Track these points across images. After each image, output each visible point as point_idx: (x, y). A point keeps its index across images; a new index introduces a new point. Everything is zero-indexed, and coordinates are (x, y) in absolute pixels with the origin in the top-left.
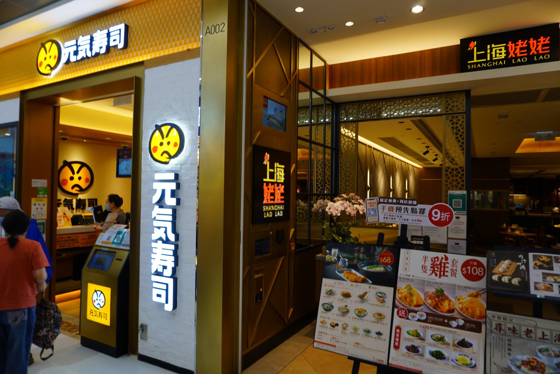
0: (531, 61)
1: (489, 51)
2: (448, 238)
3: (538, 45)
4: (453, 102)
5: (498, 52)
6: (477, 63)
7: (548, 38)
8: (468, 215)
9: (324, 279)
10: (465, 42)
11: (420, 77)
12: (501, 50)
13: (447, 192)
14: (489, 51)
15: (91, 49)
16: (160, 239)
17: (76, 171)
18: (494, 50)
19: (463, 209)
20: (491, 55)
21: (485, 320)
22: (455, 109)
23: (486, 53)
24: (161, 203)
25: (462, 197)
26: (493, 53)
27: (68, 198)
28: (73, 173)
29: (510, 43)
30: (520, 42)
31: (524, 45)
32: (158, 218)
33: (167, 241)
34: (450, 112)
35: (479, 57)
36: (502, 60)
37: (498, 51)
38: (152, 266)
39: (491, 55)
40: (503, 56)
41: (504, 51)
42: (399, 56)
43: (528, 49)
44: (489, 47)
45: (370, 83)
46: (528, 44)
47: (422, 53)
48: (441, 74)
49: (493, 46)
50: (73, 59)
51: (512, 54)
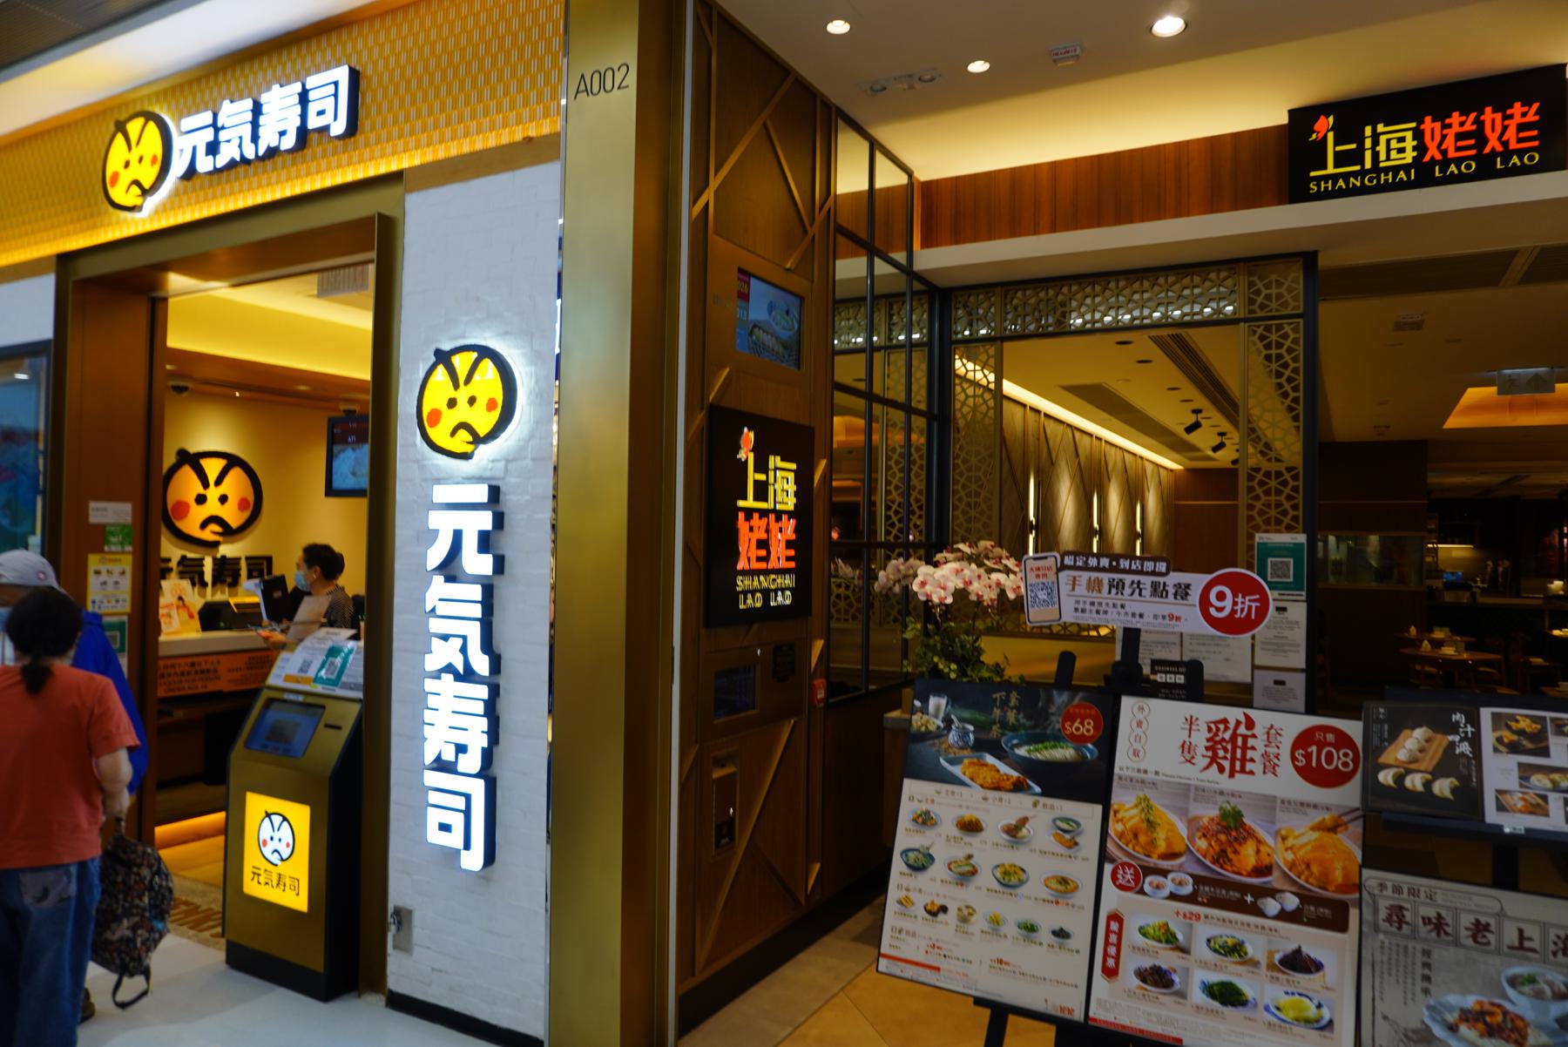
0: (1486, 170)
1: (1368, 143)
2: (1254, 667)
3: (1506, 126)
4: (1268, 286)
5: (1395, 144)
6: (1335, 177)
7: (1535, 106)
8: (1309, 601)
9: (907, 782)
10: (1302, 117)
11: (1177, 215)
12: (1402, 140)
13: (1251, 537)
14: (1368, 143)
15: (255, 138)
16: (449, 669)
18: (1383, 139)
19: (1296, 585)
20: (1375, 155)
21: (1357, 895)
22: (1274, 305)
23: (1361, 148)
24: (450, 568)
25: (1293, 550)
26: (1382, 148)
27: (190, 555)
28: (206, 485)
29: (1428, 119)
30: (1456, 118)
31: (1468, 127)
32: (442, 609)
33: (467, 675)
34: (1260, 314)
35: (1341, 159)
36: (1406, 168)
37: (1394, 144)
38: (426, 744)
39: (1375, 155)
40: (1409, 156)
41: (1410, 143)
42: (1117, 156)
43: (1479, 136)
44: (1368, 130)
45: (1036, 232)
46: (1479, 123)
47: (1180, 147)
48: (1235, 207)
49: (1380, 128)
50: (205, 164)
51: (1433, 152)
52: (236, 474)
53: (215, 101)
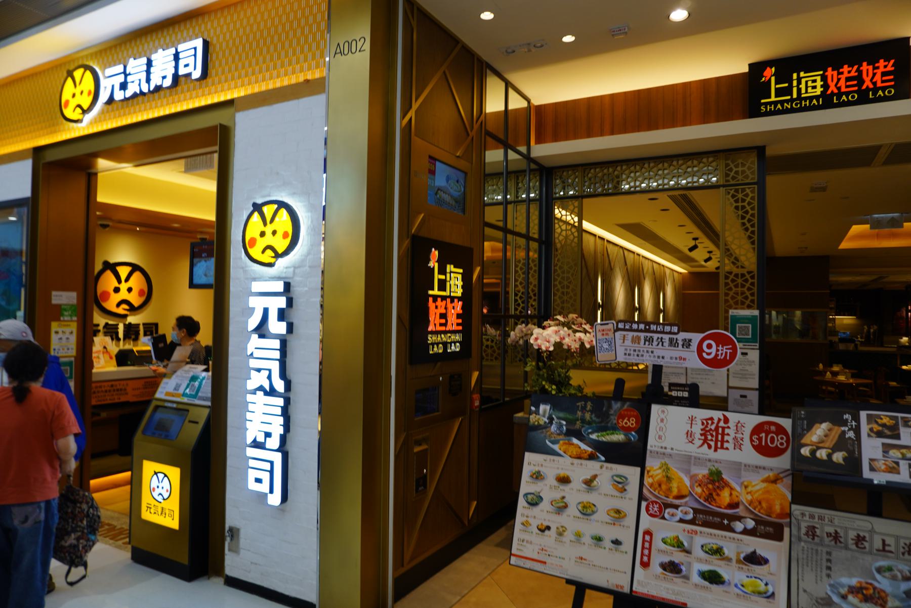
0: (864, 99)
1: (795, 83)
2: (729, 387)
3: (875, 73)
4: (737, 166)
5: (811, 84)
6: (776, 103)
7: (892, 62)
8: (761, 349)
9: (527, 454)
10: (757, 68)
11: (684, 125)
12: (814, 81)
13: (727, 312)
14: (795, 83)
15: (148, 80)
16: (261, 388)
17: (123, 277)
18: (803, 81)
19: (753, 340)
20: (799, 90)
21: (788, 520)
22: (740, 177)
23: (791, 86)
24: (261, 330)
25: (751, 320)
26: (803, 86)
27: (110, 322)
28: (119, 282)
29: (830, 69)
30: (846, 69)
31: (853, 74)
32: (257, 354)
33: (272, 392)
34: (732, 182)
35: (779, 93)
36: (817, 97)
37: (810, 84)
38: (248, 432)
39: (799, 90)
40: (819, 91)
41: (819, 83)
42: (649, 90)
43: (860, 79)
44: (795, 76)
45: (602, 135)
46: (859, 71)
47: (686, 85)
48: (718, 120)
49: (802, 74)
50: (119, 95)
51: (832, 88)
52: (137, 275)
53: (125, 59)
